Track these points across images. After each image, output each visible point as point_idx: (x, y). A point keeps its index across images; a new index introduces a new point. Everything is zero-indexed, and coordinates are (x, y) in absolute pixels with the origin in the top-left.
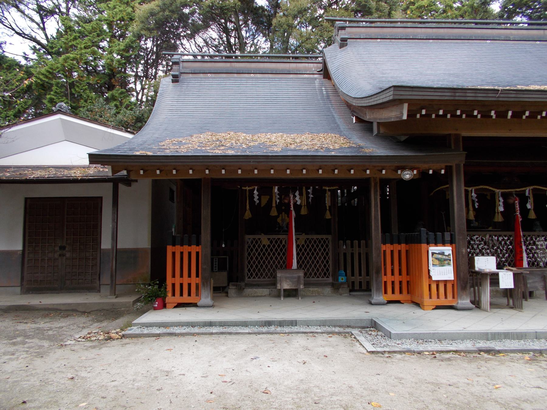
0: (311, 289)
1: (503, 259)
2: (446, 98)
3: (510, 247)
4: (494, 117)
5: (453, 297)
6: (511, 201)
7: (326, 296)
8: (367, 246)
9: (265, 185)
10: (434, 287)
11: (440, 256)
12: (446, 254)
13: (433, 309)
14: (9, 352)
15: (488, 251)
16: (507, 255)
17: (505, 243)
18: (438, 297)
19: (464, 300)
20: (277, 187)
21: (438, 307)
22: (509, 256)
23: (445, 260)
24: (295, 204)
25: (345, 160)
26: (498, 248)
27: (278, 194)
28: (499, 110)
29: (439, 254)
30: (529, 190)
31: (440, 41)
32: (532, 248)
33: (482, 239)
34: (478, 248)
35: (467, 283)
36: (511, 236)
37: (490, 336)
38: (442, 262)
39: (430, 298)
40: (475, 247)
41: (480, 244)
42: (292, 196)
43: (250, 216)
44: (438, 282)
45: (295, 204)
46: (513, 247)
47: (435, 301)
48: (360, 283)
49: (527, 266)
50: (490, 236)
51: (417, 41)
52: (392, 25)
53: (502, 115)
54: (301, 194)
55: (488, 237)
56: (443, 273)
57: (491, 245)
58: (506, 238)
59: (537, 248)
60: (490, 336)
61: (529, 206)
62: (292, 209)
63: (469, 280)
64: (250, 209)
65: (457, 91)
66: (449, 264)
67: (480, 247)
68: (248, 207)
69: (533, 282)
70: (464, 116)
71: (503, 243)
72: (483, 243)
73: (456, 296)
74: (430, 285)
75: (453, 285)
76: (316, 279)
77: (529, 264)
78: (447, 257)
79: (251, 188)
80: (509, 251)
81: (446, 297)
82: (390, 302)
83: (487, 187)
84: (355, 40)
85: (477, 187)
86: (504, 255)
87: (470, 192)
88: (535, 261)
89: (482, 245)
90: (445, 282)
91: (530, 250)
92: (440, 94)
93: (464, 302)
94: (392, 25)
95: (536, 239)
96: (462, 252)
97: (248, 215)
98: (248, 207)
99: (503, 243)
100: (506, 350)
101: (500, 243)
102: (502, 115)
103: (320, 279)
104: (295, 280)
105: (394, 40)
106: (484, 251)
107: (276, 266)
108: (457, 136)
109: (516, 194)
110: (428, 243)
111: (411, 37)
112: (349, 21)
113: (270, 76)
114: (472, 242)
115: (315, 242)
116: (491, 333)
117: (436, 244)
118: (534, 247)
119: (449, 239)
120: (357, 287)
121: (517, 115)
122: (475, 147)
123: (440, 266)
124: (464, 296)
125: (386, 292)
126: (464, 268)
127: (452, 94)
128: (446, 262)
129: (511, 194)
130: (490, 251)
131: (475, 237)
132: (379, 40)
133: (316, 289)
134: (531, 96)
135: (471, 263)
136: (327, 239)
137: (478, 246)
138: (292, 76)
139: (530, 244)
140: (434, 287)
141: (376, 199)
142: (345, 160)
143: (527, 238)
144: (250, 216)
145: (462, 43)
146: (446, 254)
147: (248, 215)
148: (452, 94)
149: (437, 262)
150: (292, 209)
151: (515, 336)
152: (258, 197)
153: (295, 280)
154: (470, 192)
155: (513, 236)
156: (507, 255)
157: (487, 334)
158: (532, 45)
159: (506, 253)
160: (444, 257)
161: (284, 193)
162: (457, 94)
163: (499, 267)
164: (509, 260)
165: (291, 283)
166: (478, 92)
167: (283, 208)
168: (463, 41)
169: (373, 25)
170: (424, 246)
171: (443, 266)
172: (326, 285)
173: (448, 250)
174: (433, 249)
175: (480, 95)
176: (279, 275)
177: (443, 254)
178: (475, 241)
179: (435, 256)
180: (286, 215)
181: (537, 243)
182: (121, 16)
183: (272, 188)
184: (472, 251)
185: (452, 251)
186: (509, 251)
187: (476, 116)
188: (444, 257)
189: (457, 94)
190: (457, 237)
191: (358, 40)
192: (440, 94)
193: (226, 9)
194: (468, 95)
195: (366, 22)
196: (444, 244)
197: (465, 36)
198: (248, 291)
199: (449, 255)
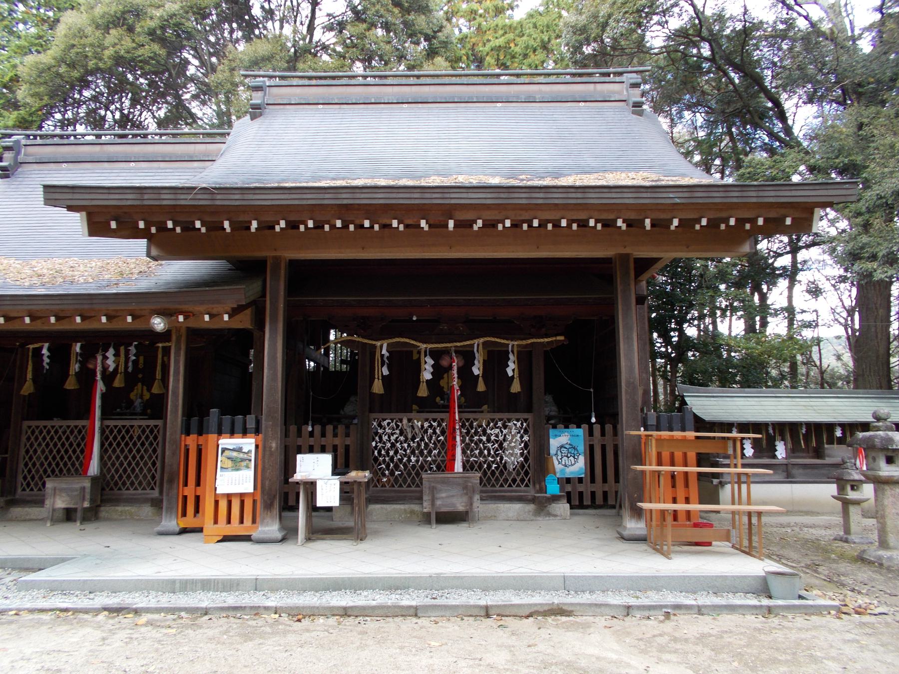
0: (119, 508)
1: (429, 459)
2: (129, 203)
3: (442, 438)
4: (228, 230)
5: (254, 522)
6: (445, 363)
7: (142, 520)
8: (615, 433)
9: (61, 343)
10: (223, 505)
11: (235, 454)
12: (245, 450)
13: (218, 541)
14: (332, 608)
15: (406, 445)
16: (436, 452)
17: (434, 432)
18: (229, 522)
19: (267, 525)
20: (79, 345)
21: (226, 539)
22: (439, 453)
23: (243, 460)
24: (105, 368)
25: (47, 302)
26: (422, 439)
27: (48, 357)
28: (240, 219)
29: (234, 450)
30: (478, 345)
31: (420, 105)
32: (481, 441)
33: (398, 426)
34: (390, 441)
35: (275, 496)
36: (442, 420)
37: (178, 585)
38: (237, 464)
39: (216, 522)
40: (385, 438)
41: (393, 434)
42: (100, 358)
43: (32, 390)
44: (229, 497)
45: (105, 368)
46: (445, 439)
47: (223, 529)
48: (593, 494)
49: (461, 470)
50: (409, 420)
51: (382, 106)
52: (436, 81)
53: (438, 226)
54: (117, 355)
55: (405, 421)
56: (234, 479)
57: (410, 436)
58: (435, 424)
59: (489, 440)
60: (178, 585)
61: (476, 371)
62: (99, 377)
63: (282, 495)
64: (34, 380)
65: (144, 191)
66: (248, 467)
67: (393, 438)
68: (29, 375)
69: (448, 497)
70: (178, 230)
71: (430, 431)
72: (398, 432)
73: (258, 519)
74: (217, 503)
75: (254, 502)
76: (132, 491)
77: (464, 467)
78: (245, 456)
79: (36, 346)
80: (439, 446)
81: (242, 522)
82: (184, 531)
83: (546, 340)
84: (282, 107)
85: (391, 341)
86: (430, 452)
87: (378, 348)
88: (485, 463)
89: (395, 436)
90: (242, 496)
91: (476, 444)
92: (117, 197)
93: (267, 529)
94: (436, 81)
95: (488, 425)
96: (271, 447)
97: (28, 388)
98: (29, 375)
99: (430, 431)
100: (363, 608)
101: (426, 431)
102: (438, 226)
103: (140, 491)
104: (76, 493)
105: (345, 106)
106: (398, 445)
107: (45, 471)
108: (277, 259)
109: (456, 352)
110: (220, 433)
111: (373, 101)
112: (279, 77)
113: (162, 164)
114: (380, 431)
115: (49, 432)
116: (180, 580)
117: (232, 433)
118: (484, 438)
119: (254, 426)
120: (587, 501)
121: (464, 225)
122: (305, 276)
123: (233, 470)
124: (268, 520)
125: (184, 514)
126: (275, 473)
127: (138, 196)
128: (244, 464)
129: (446, 352)
130: (409, 446)
131: (385, 423)
132: (321, 106)
133: (127, 508)
134: (394, 195)
135: (289, 467)
136: (156, 426)
137: (389, 437)
138: (196, 164)
139: (476, 433)
140: (223, 505)
141: (177, 362)
142: (47, 302)
143: (472, 423)
144: (32, 390)
145: (445, 108)
146: (245, 450)
147: (28, 388)
148: (138, 196)
149: (229, 464)
150: (99, 377)
151: (220, 586)
152: (48, 361)
153: (76, 493)
154: (378, 348)
155: (447, 419)
156: (436, 452)
157: (173, 582)
158: (589, 107)
159: (435, 449)
160: (241, 455)
161: (88, 354)
162: (146, 197)
163: (337, 471)
164: (439, 459)
165: (68, 498)
166: (180, 191)
167: (140, 376)
168: (458, 105)
169: (519, 81)
170: (212, 437)
171: (238, 470)
172: (145, 501)
173: (248, 444)
174: (226, 442)
175: (344, 196)
176: (49, 485)
177: (239, 450)
178: (385, 429)
179: (227, 453)
180: (145, 388)
181: (489, 431)
182: (12, 74)
183: (71, 345)
184: (380, 445)
185: (257, 446)
186: (439, 446)
187: (199, 229)
188: (241, 455)
189: (146, 197)
190: (263, 422)
191: (288, 107)
192: (117, 197)
193: (141, 61)
194: (163, 197)
195: (374, 77)
196: (245, 433)
197: (460, 98)
198: (16, 511)
199: (250, 451)
